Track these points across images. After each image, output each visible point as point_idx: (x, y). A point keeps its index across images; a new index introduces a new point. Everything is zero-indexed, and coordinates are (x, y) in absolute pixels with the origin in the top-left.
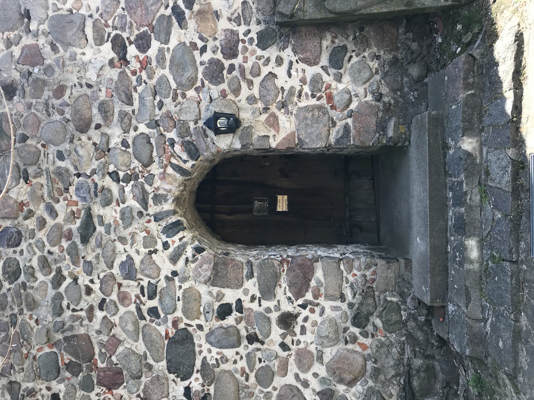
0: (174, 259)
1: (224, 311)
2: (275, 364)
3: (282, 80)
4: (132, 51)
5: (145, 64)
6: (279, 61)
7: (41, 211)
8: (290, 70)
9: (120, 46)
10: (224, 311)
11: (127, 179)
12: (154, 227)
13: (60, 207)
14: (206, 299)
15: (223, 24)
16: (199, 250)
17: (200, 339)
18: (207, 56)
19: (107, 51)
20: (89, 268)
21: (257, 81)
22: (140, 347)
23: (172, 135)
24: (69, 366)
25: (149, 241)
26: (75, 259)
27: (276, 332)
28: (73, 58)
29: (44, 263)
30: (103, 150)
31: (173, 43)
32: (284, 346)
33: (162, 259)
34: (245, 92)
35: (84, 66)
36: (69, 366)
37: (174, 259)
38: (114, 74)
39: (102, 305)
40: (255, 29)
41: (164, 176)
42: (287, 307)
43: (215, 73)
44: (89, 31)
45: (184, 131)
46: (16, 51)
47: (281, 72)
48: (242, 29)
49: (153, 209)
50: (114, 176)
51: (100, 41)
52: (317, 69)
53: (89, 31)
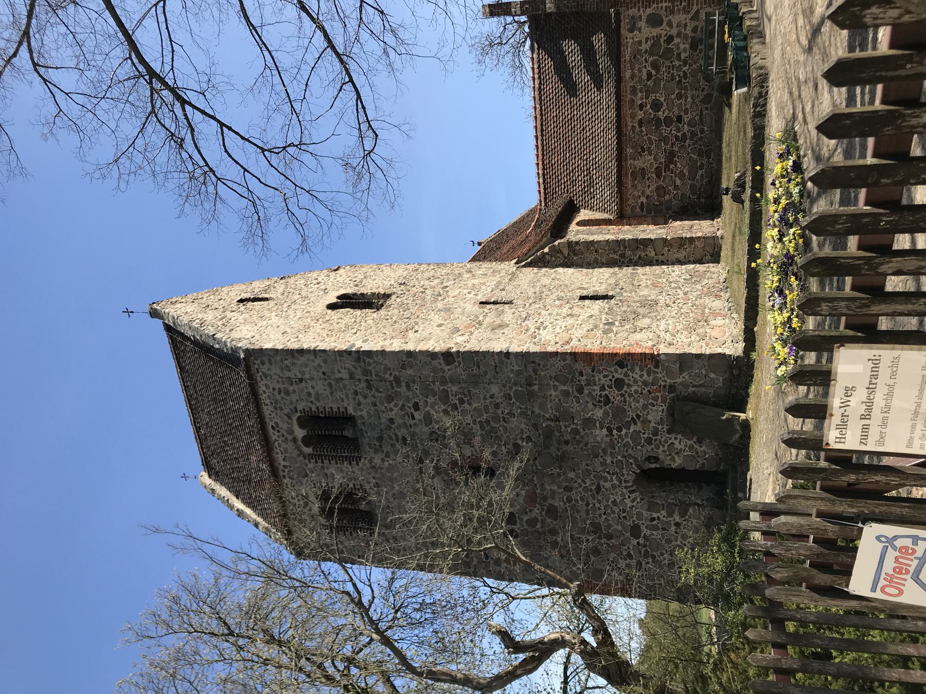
0: (633, 501)
1: (653, 519)
2: (673, 538)
3: (677, 445)
4: (615, 432)
5: (620, 436)
6: (676, 439)
7: (580, 481)
8: (681, 443)
9: (610, 430)
10: (653, 519)
11: (613, 474)
12: (624, 490)
13: (588, 481)
14: (645, 515)
15: (652, 424)
16: (642, 499)
17: (643, 528)
18: (646, 436)
19: (605, 431)
20: (599, 502)
21: (666, 445)
22: (620, 528)
23: (631, 461)
24: (593, 532)
25: (623, 495)
26: (594, 498)
27: (673, 528)
28: (592, 433)
29: (582, 499)
30: (604, 464)
31: (631, 430)
32: (676, 532)
33: (628, 501)
34: (661, 448)
35: (596, 436)
36: (593, 532)
37: (633, 501)
38: (608, 439)
39: (605, 514)
40: (666, 428)
41: (628, 474)
42: (677, 520)
43: (649, 441)
44: (598, 425)
45: (636, 459)
46: (569, 430)
47: (677, 442)
48: (660, 427)
49: (624, 485)
50: (608, 472)
51: (602, 428)
52: (692, 442)
53: (598, 425)
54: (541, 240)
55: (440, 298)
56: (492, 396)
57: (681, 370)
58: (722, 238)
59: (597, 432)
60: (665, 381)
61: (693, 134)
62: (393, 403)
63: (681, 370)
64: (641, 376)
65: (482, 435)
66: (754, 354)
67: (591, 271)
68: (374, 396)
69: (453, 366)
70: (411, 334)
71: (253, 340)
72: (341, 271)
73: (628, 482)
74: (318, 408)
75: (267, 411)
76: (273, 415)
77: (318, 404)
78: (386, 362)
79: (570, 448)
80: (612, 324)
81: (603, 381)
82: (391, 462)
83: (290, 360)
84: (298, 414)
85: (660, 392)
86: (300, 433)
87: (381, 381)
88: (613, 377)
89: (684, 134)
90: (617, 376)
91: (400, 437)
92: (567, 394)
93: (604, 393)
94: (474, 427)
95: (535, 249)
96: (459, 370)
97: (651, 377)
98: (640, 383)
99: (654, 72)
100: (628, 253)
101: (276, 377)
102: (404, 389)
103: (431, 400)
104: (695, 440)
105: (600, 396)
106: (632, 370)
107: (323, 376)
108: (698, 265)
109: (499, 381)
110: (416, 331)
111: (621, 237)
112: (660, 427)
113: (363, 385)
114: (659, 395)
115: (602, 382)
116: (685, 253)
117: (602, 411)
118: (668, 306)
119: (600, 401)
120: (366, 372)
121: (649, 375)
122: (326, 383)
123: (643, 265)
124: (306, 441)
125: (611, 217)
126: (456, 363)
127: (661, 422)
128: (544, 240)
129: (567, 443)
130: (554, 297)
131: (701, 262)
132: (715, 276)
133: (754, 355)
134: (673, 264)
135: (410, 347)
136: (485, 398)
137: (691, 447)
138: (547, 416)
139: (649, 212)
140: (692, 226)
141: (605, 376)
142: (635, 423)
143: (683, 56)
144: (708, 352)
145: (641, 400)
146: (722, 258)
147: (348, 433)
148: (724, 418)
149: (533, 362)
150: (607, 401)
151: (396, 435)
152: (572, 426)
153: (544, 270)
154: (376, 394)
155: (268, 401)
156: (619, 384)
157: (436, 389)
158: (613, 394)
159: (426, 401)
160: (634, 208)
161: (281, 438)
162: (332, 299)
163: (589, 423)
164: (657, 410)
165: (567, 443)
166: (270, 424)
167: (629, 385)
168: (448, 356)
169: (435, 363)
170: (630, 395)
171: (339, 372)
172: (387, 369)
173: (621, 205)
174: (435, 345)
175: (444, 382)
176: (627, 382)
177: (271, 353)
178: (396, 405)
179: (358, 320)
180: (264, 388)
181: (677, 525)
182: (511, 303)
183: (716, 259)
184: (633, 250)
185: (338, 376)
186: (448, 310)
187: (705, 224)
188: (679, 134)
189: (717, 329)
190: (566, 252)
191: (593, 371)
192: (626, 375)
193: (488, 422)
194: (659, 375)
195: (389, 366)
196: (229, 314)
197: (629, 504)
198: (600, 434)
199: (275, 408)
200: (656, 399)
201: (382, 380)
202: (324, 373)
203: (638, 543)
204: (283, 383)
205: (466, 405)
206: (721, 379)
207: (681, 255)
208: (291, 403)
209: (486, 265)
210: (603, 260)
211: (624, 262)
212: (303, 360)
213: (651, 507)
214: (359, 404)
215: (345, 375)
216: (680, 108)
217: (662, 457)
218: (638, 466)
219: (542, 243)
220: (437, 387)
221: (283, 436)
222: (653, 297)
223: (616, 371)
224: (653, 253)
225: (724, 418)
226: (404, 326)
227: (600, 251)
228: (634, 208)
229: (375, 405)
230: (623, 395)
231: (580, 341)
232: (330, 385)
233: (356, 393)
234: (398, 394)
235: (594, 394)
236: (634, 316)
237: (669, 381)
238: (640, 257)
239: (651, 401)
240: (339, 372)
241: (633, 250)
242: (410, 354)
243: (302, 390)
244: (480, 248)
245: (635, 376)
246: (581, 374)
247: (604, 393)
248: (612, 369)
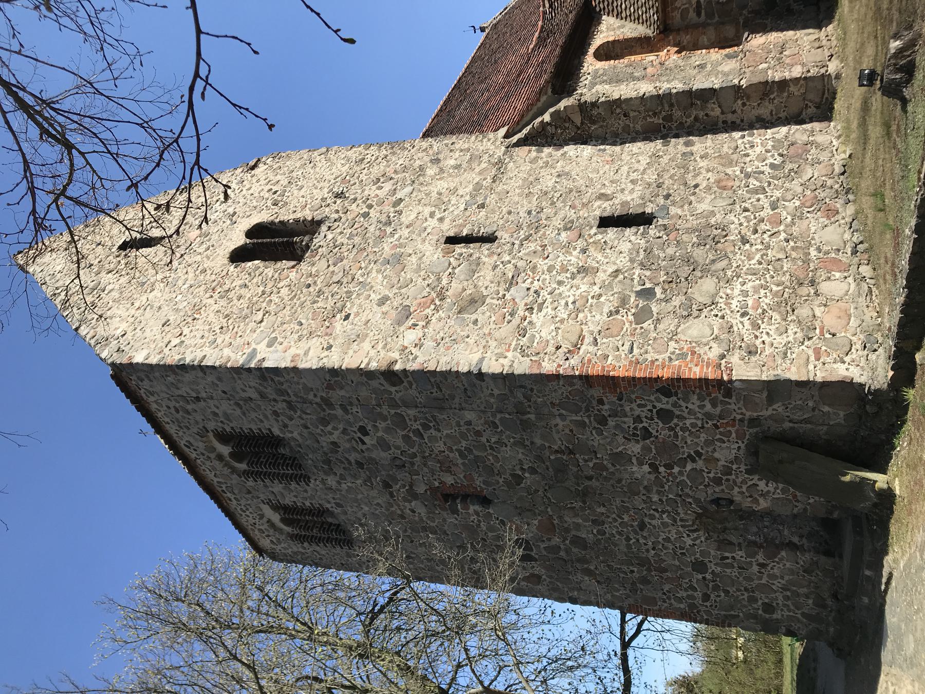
9: (654, 467)
11: (663, 512)
18: (711, 475)
19: (646, 468)
23: (690, 500)
25: (678, 532)
34: (736, 489)
38: (652, 477)
39: (654, 549)
43: (718, 481)
46: (591, 464)
51: (641, 464)
54: (538, 100)
55: (389, 230)
56: (469, 423)
57: (771, 400)
58: (838, 77)
59: (635, 469)
63: (771, 400)
65: (463, 464)
66: (912, 392)
67: (618, 149)
70: (339, 325)
72: (262, 167)
73: (687, 521)
74: (232, 428)
76: (181, 434)
77: (231, 425)
78: (303, 380)
79: (594, 483)
81: (637, 411)
82: (349, 484)
85: (733, 426)
88: (654, 407)
90: (659, 406)
91: (353, 461)
92: (582, 425)
94: (451, 455)
95: (531, 114)
96: (413, 392)
97: (719, 409)
100: (677, 113)
102: (339, 412)
106: (686, 400)
108: (794, 128)
109: (475, 406)
111: (665, 86)
112: (734, 467)
114: (733, 430)
116: (771, 107)
117: (639, 446)
118: (745, 241)
121: (714, 405)
123: (702, 133)
125: (649, 32)
126: (405, 384)
128: (544, 98)
129: (590, 478)
130: (557, 222)
131: (798, 119)
132: (824, 156)
133: (911, 394)
134: (751, 127)
135: (334, 360)
136: (458, 425)
138: (556, 448)
139: (710, 15)
140: (783, 49)
144: (819, 379)
145: (702, 435)
146: (836, 114)
148: (847, 478)
149: (521, 387)
150: (647, 434)
151: (347, 459)
152: (594, 461)
153: (547, 150)
154: (304, 416)
155: (167, 420)
156: (665, 415)
160: (685, 12)
162: (238, 239)
163: (620, 458)
164: (729, 448)
165: (590, 478)
166: (182, 443)
168: (390, 375)
169: (374, 383)
170: (683, 429)
173: (664, 11)
174: (366, 355)
175: (394, 404)
177: (145, 369)
178: (335, 428)
179: (268, 290)
181: (762, 566)
182: (490, 239)
183: (824, 113)
184: (685, 108)
186: (397, 260)
187: (804, 38)
189: (835, 308)
190: (578, 120)
191: (620, 399)
193: (469, 450)
194: (733, 406)
195: (309, 386)
198: (641, 471)
202: (224, 392)
203: (704, 578)
205: (432, 431)
206: (842, 414)
207: (765, 111)
208: (197, 423)
209: (462, 142)
210: (638, 127)
211: (670, 128)
212: (188, 377)
213: (724, 544)
214: (286, 426)
217: (738, 499)
219: (539, 104)
221: (203, 455)
222: (719, 217)
223: (659, 401)
224: (718, 111)
225: (847, 478)
227: (632, 114)
228: (685, 12)
229: (307, 428)
230: (671, 429)
233: (275, 413)
236: (687, 270)
238: (696, 119)
239: (718, 436)
241: (685, 108)
242: (334, 372)
244: (485, 34)
245: (690, 406)
248: (652, 398)
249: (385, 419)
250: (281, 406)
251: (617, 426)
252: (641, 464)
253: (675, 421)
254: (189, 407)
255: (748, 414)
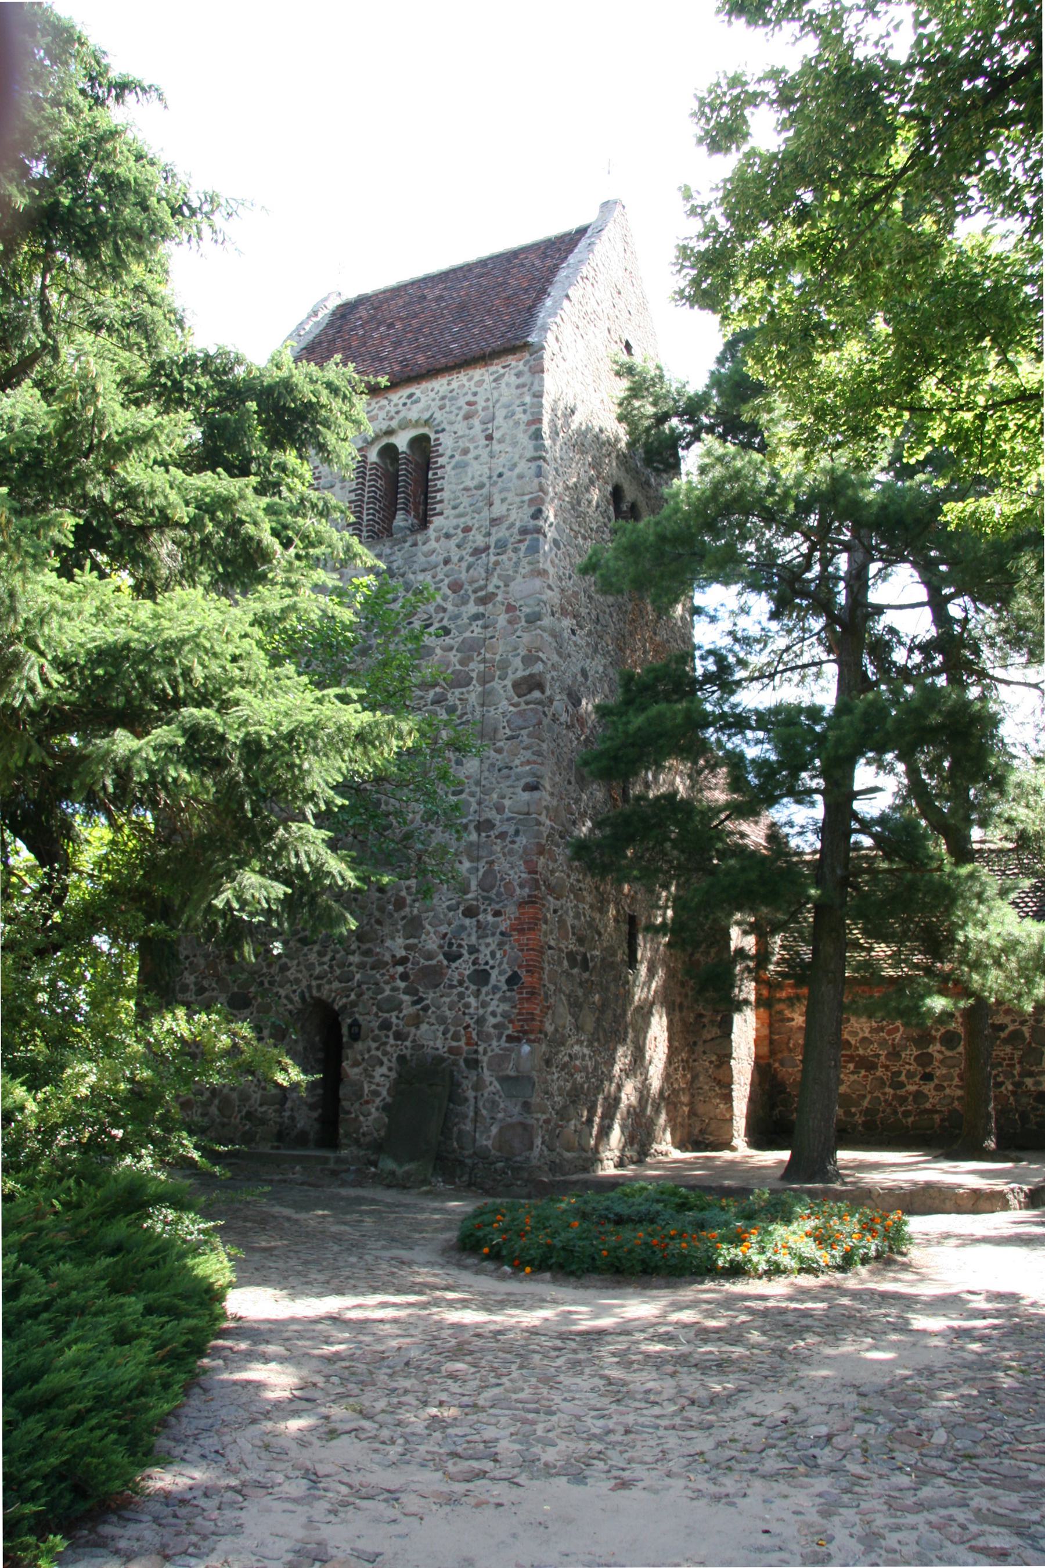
4: (400, 969)
5: (393, 977)
6: (390, 1069)
8: (383, 1076)
9: (403, 961)
18: (394, 1020)
23: (353, 996)
25: (297, 981)
37: (287, 997)
38: (387, 958)
43: (386, 1026)
44: (411, 941)
45: (354, 1004)
46: (404, 893)
49: (314, 983)
51: (407, 948)
52: (384, 1093)
53: (411, 941)
57: (504, 1080)
60: (485, 1052)
61: (903, 1100)
62: (449, 592)
64: (494, 1014)
68: (461, 559)
69: (511, 692)
71: (558, 359)
75: (440, 385)
76: (432, 395)
77: (448, 468)
78: (519, 579)
80: (585, 967)
83: (525, 418)
84: (433, 436)
86: (401, 441)
87: (487, 571)
89: (902, 1085)
90: (494, 974)
93: (464, 952)
98: (481, 1011)
99: (1003, 1035)
101: (496, 394)
102: (472, 608)
103: (454, 657)
104: (389, 1100)
105: (460, 946)
106: (503, 999)
107: (495, 474)
110: (573, 632)
112: (408, 1043)
113: (480, 541)
114: (462, 1043)
115: (482, 948)
117: (435, 947)
119: (450, 945)
120: (502, 546)
121: (495, 1026)
122: (485, 480)
124: (389, 452)
126: (516, 699)
127: (417, 1047)
137: (376, 1093)
141: (493, 954)
142: (415, 1003)
143: (1029, 1081)
147: (400, 520)
150: (452, 957)
154: (464, 565)
157: (472, 665)
158: (464, 967)
159: (451, 649)
161: (393, 410)
163: (414, 927)
167: (477, 994)
170: (461, 996)
171: (503, 500)
172: (507, 581)
175: (484, 680)
176: (484, 990)
178: (445, 598)
180: (477, 378)
185: (497, 499)
188: (903, 1078)
192: (496, 989)
194: (494, 1043)
196: (603, 325)
197: (282, 992)
199: (443, 398)
200: (456, 1037)
201: (489, 573)
202: (500, 475)
204: (484, 409)
215: (498, 509)
216: (944, 1077)
217: (359, 1046)
218: (344, 1006)
220: (475, 667)
226: (584, 611)
229: (446, 562)
230: (461, 983)
231: (555, 911)
232: (481, 486)
233: (467, 530)
234: (464, 602)
235: (464, 935)
237: (485, 1059)
239: (452, 1029)
240: (503, 500)
243: (472, 440)
245: (495, 1003)
246: (497, 914)
247: (464, 952)
248: (505, 966)
249: (463, 662)
250: (478, 539)
251: (463, 928)
252: (407, 948)
253: (473, 987)
254: (476, 422)
255: (485, 1059)
